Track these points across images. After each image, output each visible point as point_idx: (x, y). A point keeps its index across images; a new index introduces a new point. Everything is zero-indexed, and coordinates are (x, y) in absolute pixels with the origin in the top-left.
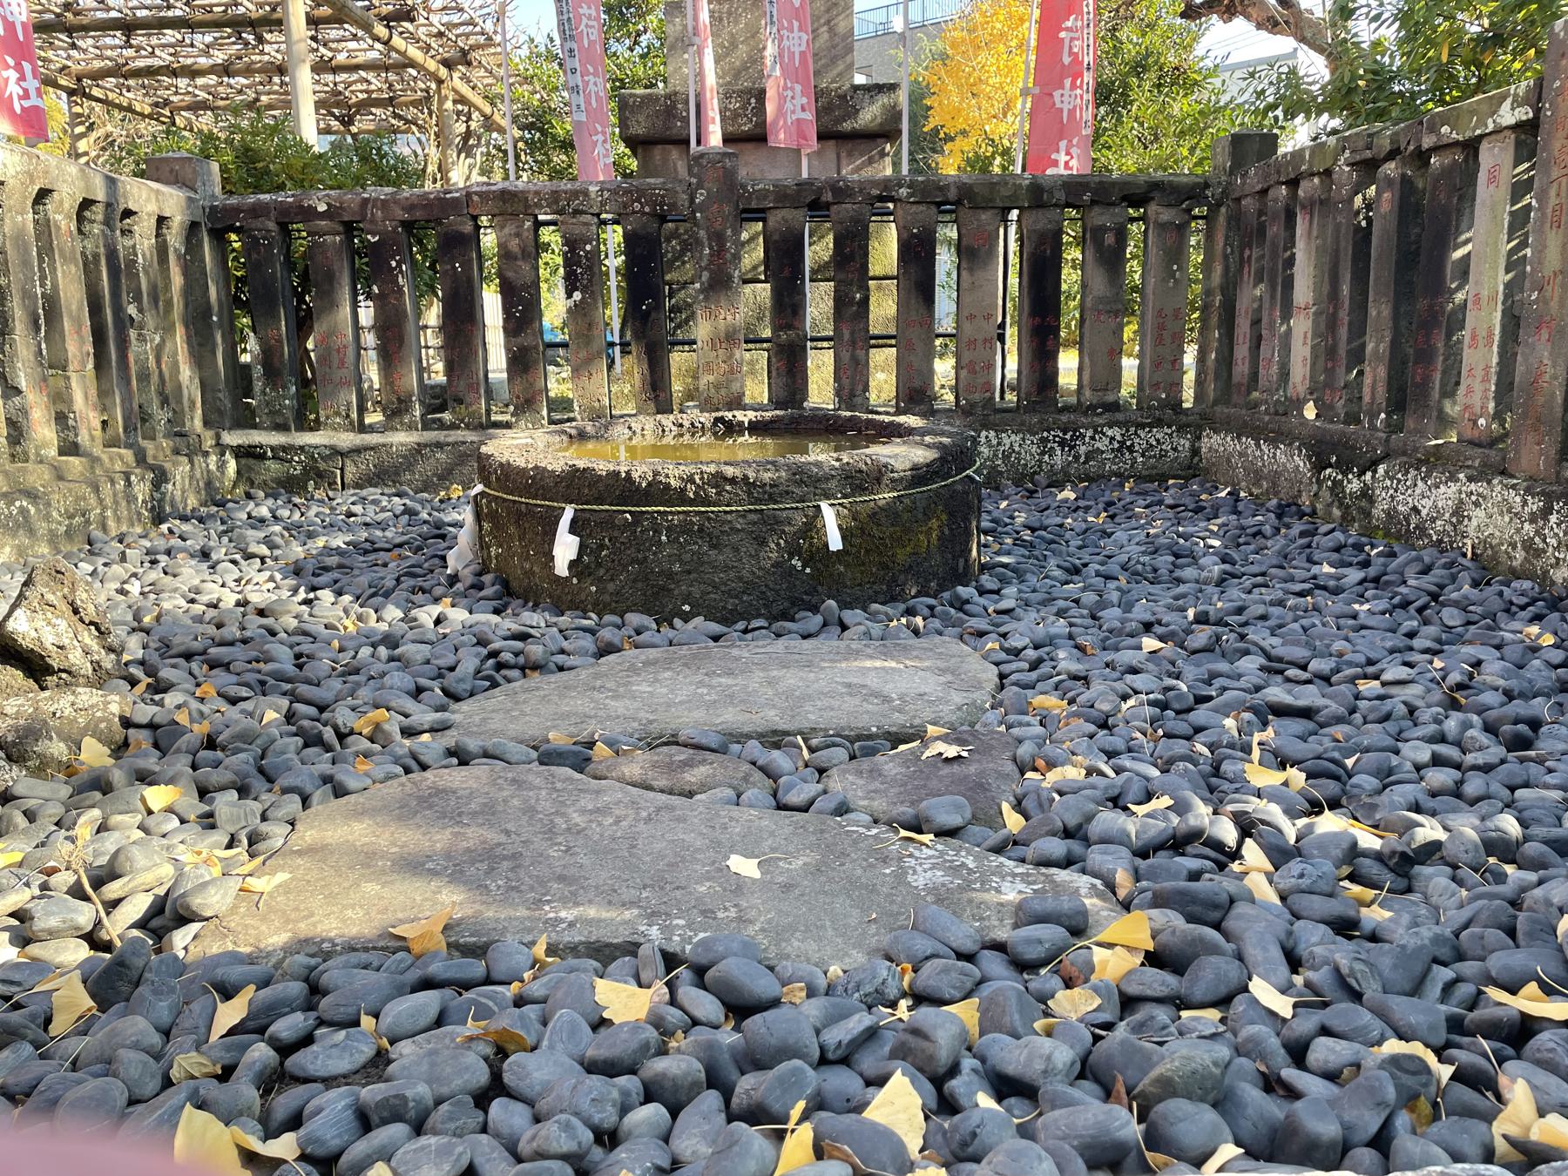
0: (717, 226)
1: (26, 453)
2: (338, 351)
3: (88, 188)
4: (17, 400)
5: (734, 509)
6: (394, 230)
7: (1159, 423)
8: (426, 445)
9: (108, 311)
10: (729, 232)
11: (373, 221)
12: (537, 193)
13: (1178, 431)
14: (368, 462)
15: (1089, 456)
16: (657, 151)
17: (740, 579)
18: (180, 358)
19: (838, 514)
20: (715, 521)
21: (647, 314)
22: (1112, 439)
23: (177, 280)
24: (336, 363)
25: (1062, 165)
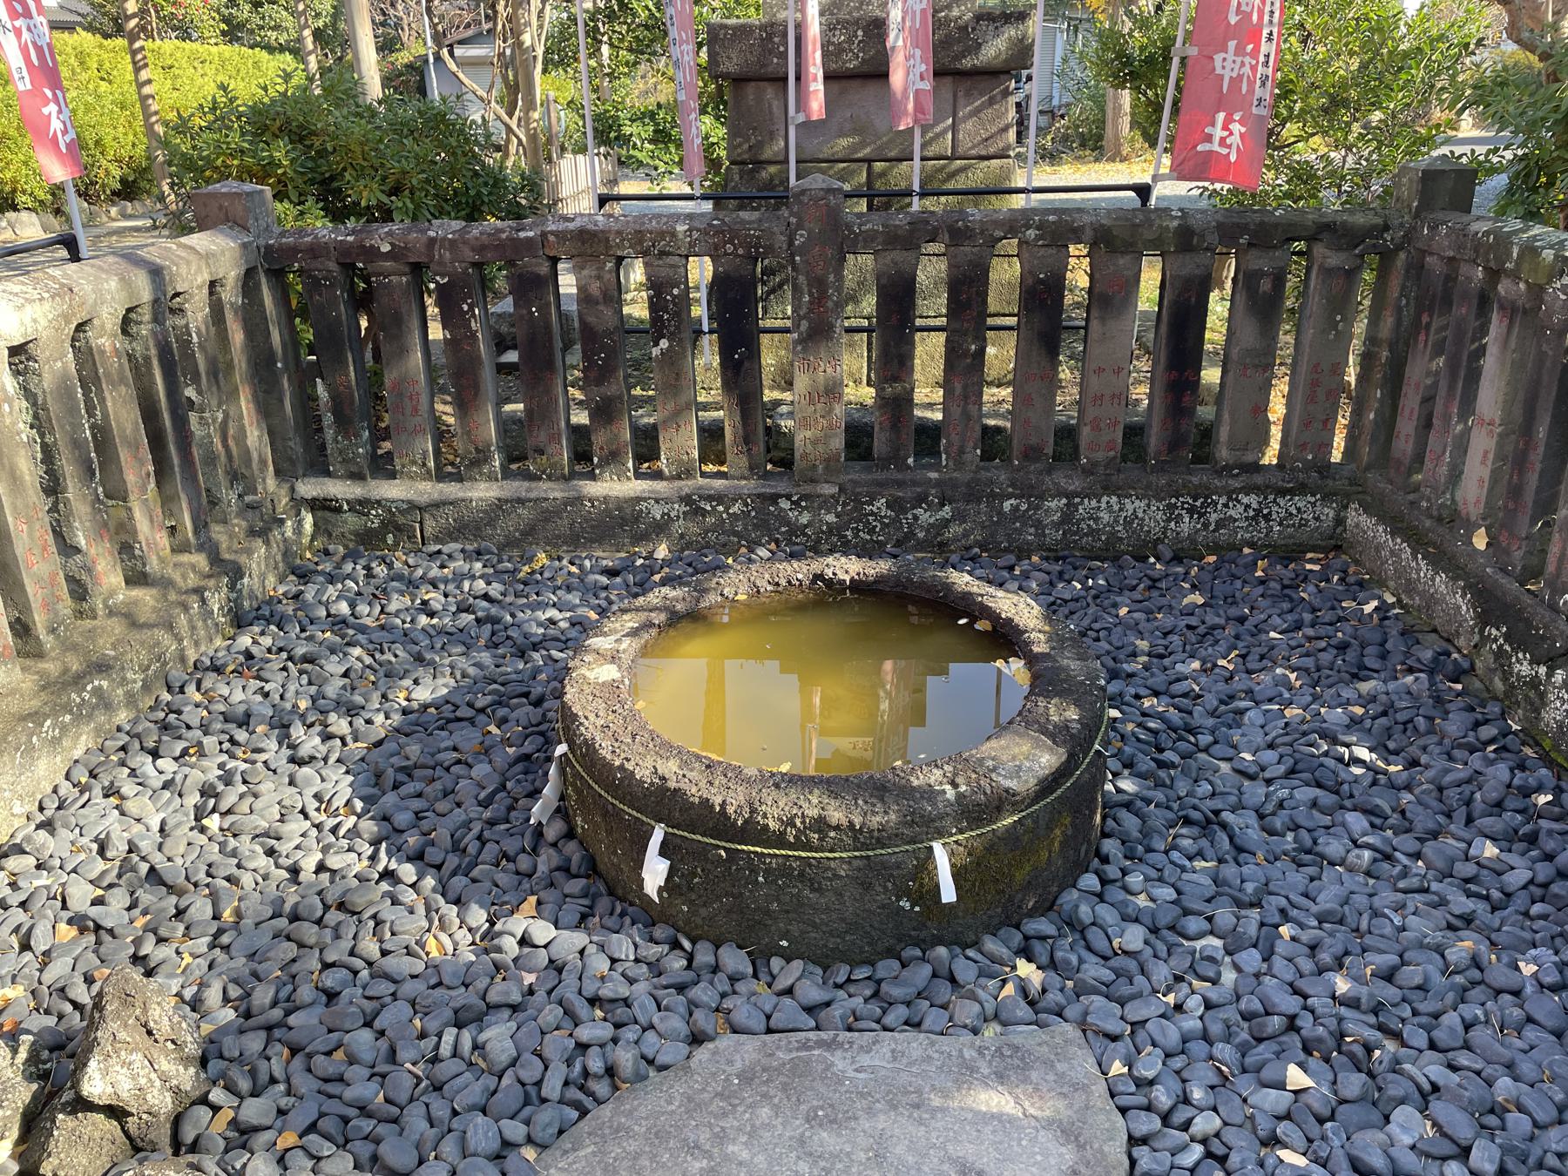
0: (819, 271)
1: (93, 610)
2: (411, 398)
3: (131, 296)
4: (78, 558)
5: (840, 857)
6: (465, 270)
7: (1302, 489)
8: (507, 501)
9: (166, 416)
10: (831, 278)
11: (440, 263)
12: (619, 233)
13: (1323, 499)
14: (448, 517)
15: (1220, 524)
16: (751, 89)
17: (843, 920)
18: (246, 422)
19: (952, 854)
20: (817, 867)
21: (740, 363)
22: (1248, 506)
23: (237, 336)
24: (408, 411)
25: (1216, 140)
